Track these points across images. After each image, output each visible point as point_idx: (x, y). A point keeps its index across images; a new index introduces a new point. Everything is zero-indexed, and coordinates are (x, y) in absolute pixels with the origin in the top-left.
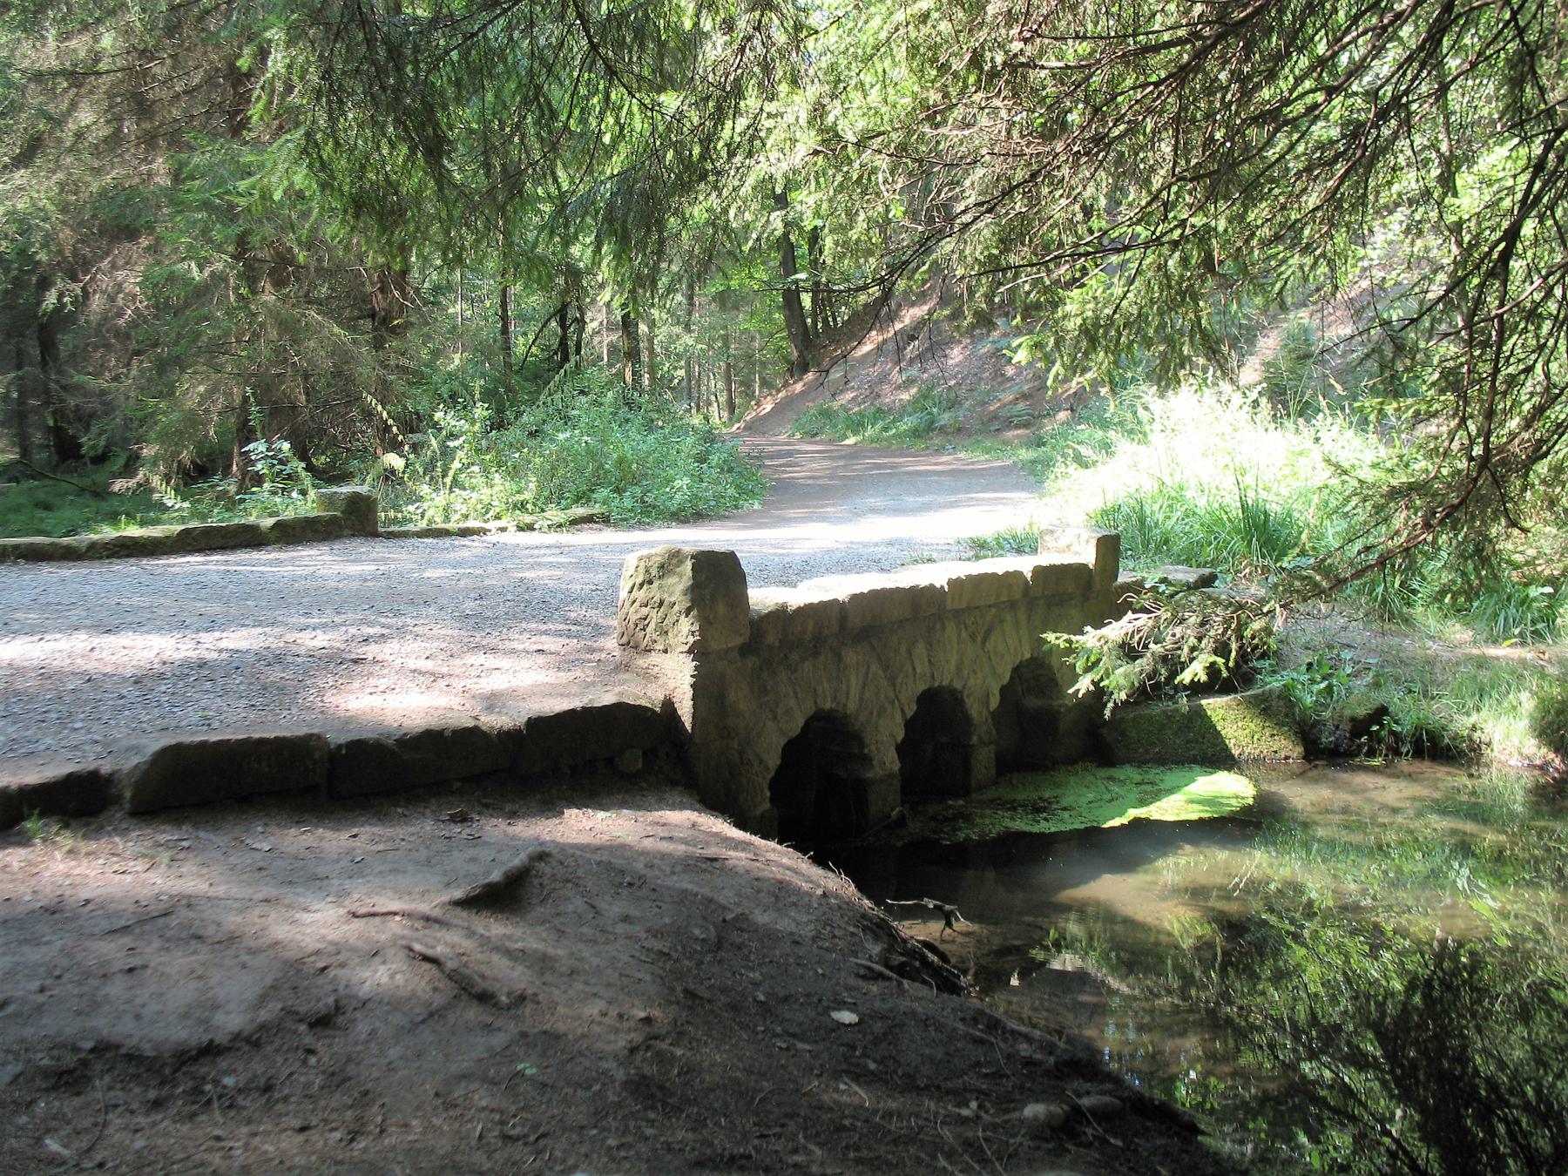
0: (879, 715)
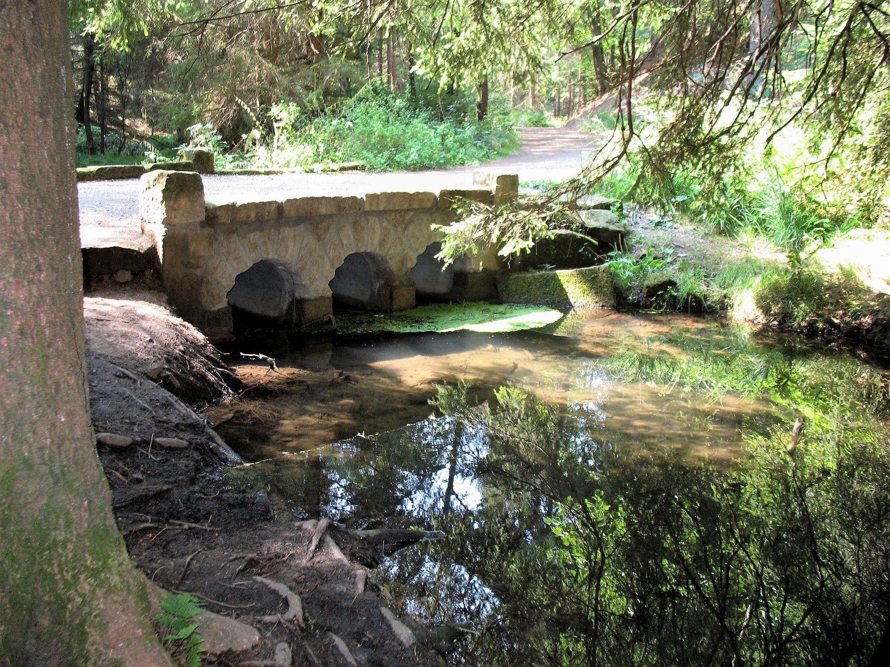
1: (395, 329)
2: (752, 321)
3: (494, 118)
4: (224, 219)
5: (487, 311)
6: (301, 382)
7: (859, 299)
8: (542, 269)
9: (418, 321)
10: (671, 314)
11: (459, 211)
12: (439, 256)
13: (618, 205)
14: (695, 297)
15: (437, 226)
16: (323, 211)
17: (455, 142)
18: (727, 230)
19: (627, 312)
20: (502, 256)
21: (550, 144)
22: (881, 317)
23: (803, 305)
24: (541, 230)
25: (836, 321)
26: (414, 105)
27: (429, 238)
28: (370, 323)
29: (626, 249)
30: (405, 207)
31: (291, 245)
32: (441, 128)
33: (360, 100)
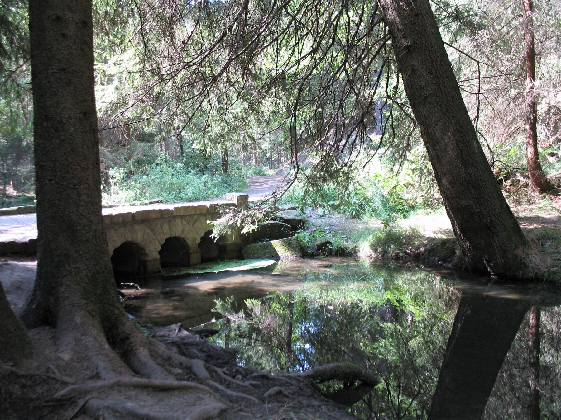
0: (150, 243)
1: (193, 272)
3: (233, 171)
5: (238, 263)
6: (151, 293)
7: (419, 240)
8: (264, 241)
9: (204, 269)
10: (329, 257)
11: (221, 212)
12: (212, 235)
13: (300, 207)
14: (341, 248)
16: (154, 216)
17: (212, 185)
18: (357, 216)
19: (308, 258)
20: (243, 233)
21: (267, 184)
22: (428, 247)
23: (392, 246)
25: (409, 252)
26: (187, 165)
27: (206, 228)
28: (180, 271)
29: (305, 229)
30: (193, 213)
31: (139, 233)
33: (157, 164)
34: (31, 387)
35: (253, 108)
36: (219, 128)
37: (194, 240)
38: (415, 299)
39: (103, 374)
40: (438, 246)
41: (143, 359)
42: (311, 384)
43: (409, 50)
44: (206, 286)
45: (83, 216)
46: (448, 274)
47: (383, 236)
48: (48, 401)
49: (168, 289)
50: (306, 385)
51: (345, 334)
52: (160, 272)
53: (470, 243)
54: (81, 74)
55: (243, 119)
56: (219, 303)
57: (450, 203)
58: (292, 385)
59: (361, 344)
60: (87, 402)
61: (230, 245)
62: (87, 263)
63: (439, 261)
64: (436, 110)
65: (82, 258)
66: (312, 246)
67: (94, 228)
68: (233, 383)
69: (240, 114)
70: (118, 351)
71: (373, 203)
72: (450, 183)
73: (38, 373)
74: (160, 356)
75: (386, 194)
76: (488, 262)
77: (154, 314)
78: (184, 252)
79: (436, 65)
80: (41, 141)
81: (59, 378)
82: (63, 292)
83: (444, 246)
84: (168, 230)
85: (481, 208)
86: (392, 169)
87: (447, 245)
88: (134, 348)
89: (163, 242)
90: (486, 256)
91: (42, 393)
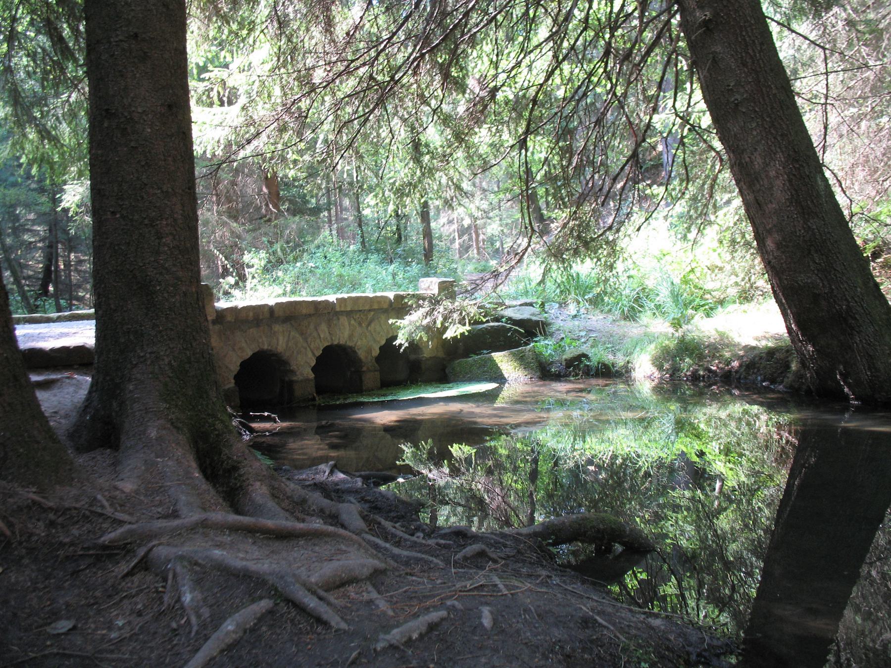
1: (366, 400)
2: (650, 377)
4: (229, 318)
8: (480, 354)
9: (384, 395)
15: (394, 321)
16: (304, 311)
18: (631, 315)
19: (552, 380)
22: (745, 359)
24: (475, 315)
26: (365, 248)
28: (345, 399)
29: (546, 335)
30: (367, 308)
31: (281, 338)
32: (391, 268)
33: (318, 247)
34: (63, 526)
35: (460, 137)
36: (407, 171)
37: (369, 351)
38: (727, 451)
39: (184, 511)
40: (761, 358)
41: (259, 499)
42: (538, 547)
43: (708, 29)
44: (385, 417)
45: (166, 269)
46: (777, 398)
47: (672, 344)
48: (88, 549)
49: (324, 423)
50: (530, 547)
51: (611, 503)
52: (314, 399)
53: (814, 346)
54: (163, 44)
55: (445, 156)
56: (407, 450)
57: (780, 279)
58: (505, 546)
59: (638, 520)
60: (151, 550)
61: (427, 359)
62: (171, 346)
63: (764, 381)
64: (754, 125)
65: (162, 336)
66: (558, 361)
67: (184, 289)
68: (406, 540)
69: (440, 150)
70: (220, 489)
71: (658, 295)
72: (779, 246)
73: (77, 506)
74: (288, 498)
75: (677, 281)
76: (844, 376)
77: (299, 454)
78: (353, 369)
79: (753, 51)
80: (100, 152)
81: (110, 515)
82: (131, 391)
83: (772, 358)
84: (327, 334)
85: (830, 287)
86: (685, 237)
87: (777, 355)
88: (245, 484)
89: (319, 353)
90: (841, 367)
91: (80, 535)
